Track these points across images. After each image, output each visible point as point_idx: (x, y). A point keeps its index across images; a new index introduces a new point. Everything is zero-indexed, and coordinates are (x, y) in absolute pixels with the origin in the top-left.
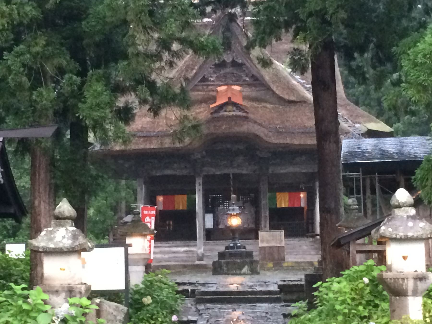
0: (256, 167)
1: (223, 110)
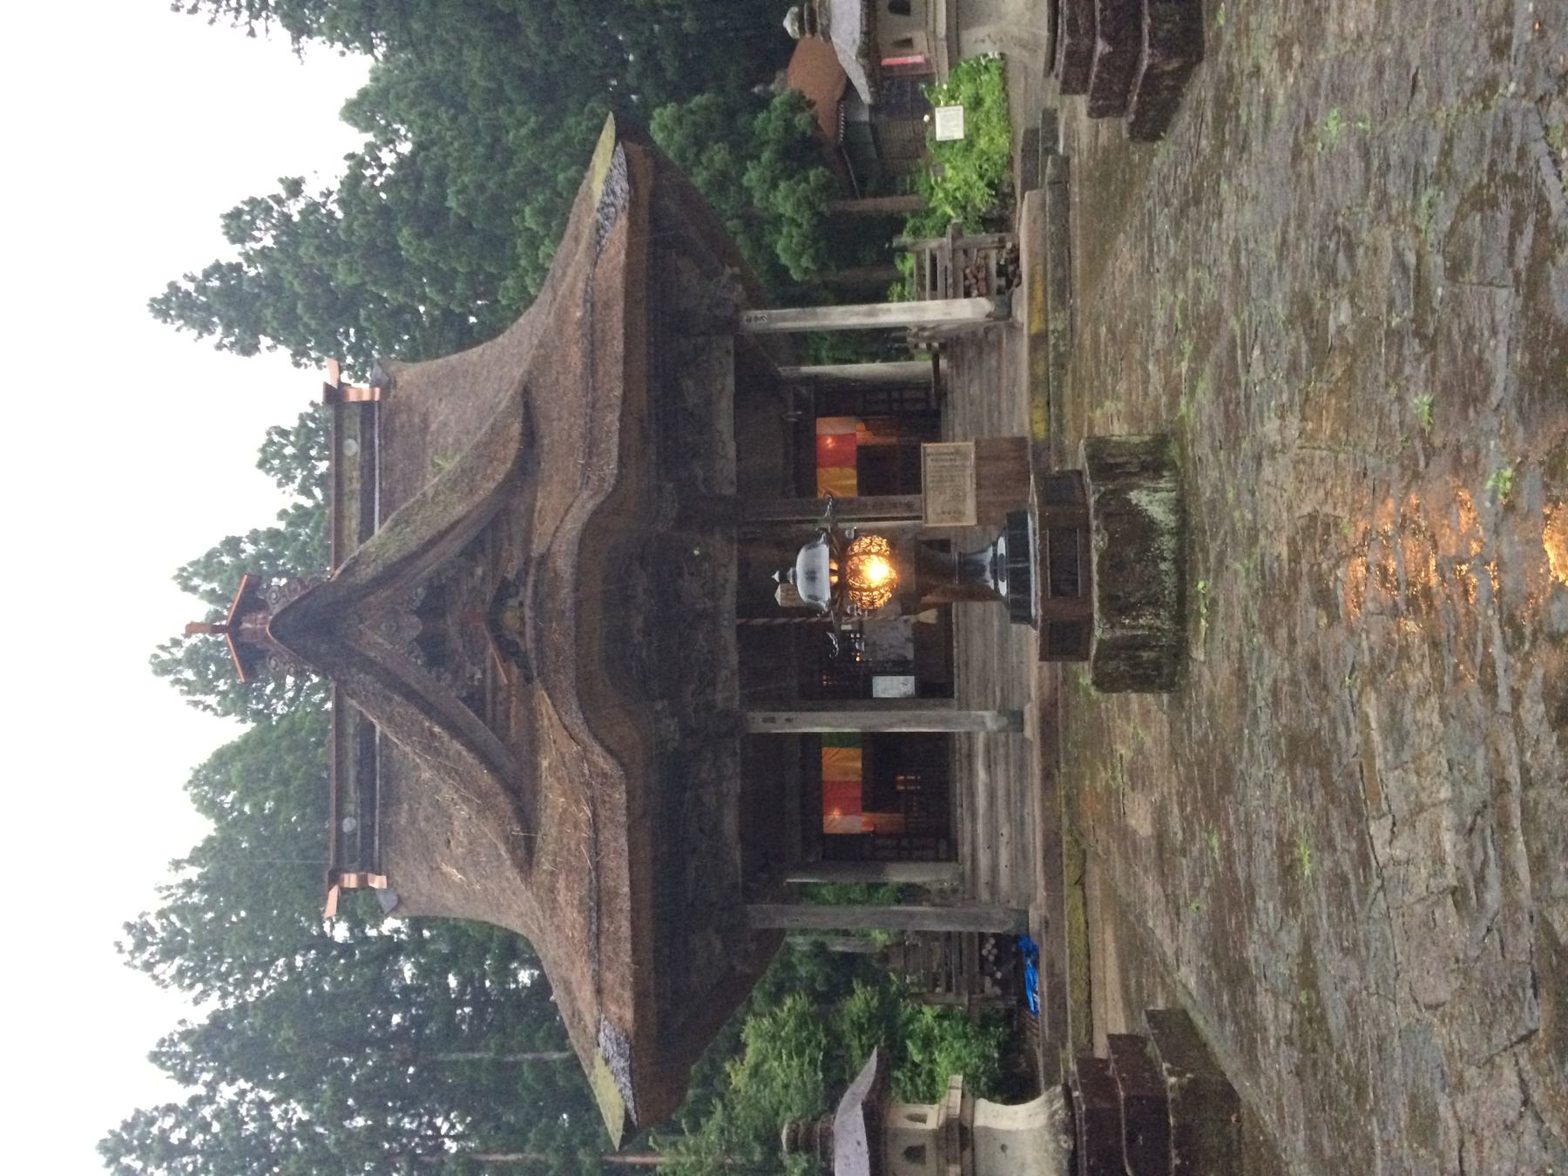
1: (518, 640)
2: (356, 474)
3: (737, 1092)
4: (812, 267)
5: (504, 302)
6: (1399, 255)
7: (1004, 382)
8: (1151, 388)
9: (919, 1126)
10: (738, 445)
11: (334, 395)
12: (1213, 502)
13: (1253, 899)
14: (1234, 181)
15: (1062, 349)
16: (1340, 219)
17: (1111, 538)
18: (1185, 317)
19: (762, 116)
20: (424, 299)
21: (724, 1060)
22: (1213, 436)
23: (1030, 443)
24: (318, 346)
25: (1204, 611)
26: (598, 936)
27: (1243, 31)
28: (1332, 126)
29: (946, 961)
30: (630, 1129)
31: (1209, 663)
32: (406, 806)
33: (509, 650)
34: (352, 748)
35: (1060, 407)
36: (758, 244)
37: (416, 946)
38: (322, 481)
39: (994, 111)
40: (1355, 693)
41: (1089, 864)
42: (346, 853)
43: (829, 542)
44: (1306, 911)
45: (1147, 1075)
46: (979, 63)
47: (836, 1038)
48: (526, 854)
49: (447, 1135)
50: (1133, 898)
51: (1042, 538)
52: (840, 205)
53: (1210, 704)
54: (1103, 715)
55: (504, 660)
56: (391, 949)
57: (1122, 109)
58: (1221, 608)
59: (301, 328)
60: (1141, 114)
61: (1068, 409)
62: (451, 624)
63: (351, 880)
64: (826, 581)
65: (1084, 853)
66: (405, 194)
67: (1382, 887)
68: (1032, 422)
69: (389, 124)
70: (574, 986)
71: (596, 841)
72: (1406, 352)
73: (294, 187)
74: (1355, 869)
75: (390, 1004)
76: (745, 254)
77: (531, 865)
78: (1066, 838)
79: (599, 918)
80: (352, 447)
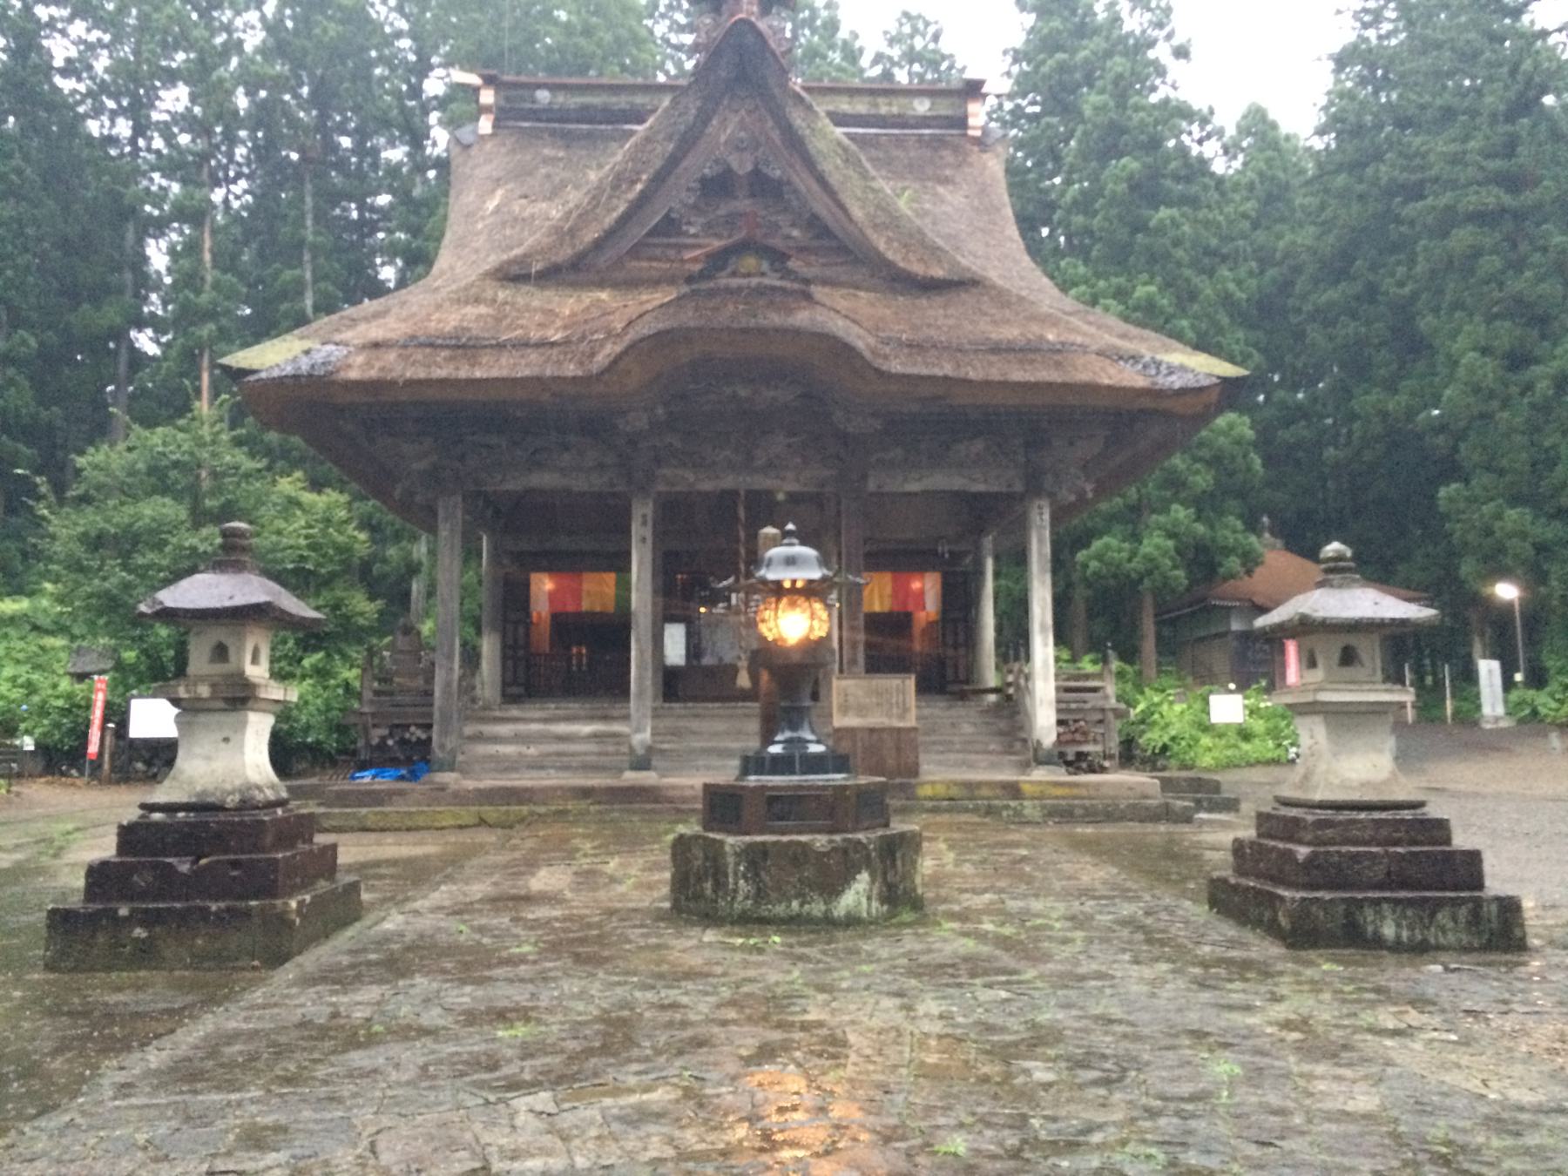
0: (826, 473)
1: (729, 270)
2: (895, 110)
3: (274, 482)
4: (1089, 572)
5: (1063, 264)
6: (1100, 1127)
7: (973, 757)
8: (967, 896)
9: (248, 657)
10: (916, 494)
11: (973, 89)
12: (857, 952)
13: (472, 983)
14: (1170, 976)
15: (1005, 813)
16: (1133, 1073)
17: (825, 854)
18: (1036, 928)
19: (1239, 525)
20: (1068, 182)
21: (305, 472)
22: (924, 952)
23: (913, 781)
24: (1023, 74)
25: (752, 941)
26: (431, 345)
27: (1316, 987)
28: (1224, 1067)
29: (403, 690)
30: (240, 374)
31: (701, 946)
32: (561, 154)
33: (718, 261)
34: (621, 102)
35: (949, 810)
36: (1112, 518)
37: (419, 164)
38: (887, 75)
39: (1237, 753)
40: (675, 1080)
41: (499, 831)
42: (513, 93)
43: (824, 579)
44: (464, 1032)
45: (298, 880)
46: (1286, 738)
47: (327, 582)
48: (512, 275)
49: (229, 191)
50: (468, 871)
51: (824, 788)
52: (1148, 602)
53: (658, 947)
54: (647, 847)
55: (708, 256)
56: (416, 137)
57: (1240, 871)
58: (755, 958)
59: (1042, 56)
60: (1235, 888)
61: (945, 818)
62: (743, 204)
63: (487, 97)
64: (786, 576)
65: (511, 827)
66: (1173, 165)
67: (487, 1102)
68: (933, 783)
69: (1243, 150)
70: (382, 321)
71: (526, 345)
72: (1006, 1132)
73: (1181, 53)
74: (505, 1078)
75: (361, 135)
76: (1104, 506)
77: (500, 280)
78: (525, 809)
79: (447, 347)
80: (922, 107)
